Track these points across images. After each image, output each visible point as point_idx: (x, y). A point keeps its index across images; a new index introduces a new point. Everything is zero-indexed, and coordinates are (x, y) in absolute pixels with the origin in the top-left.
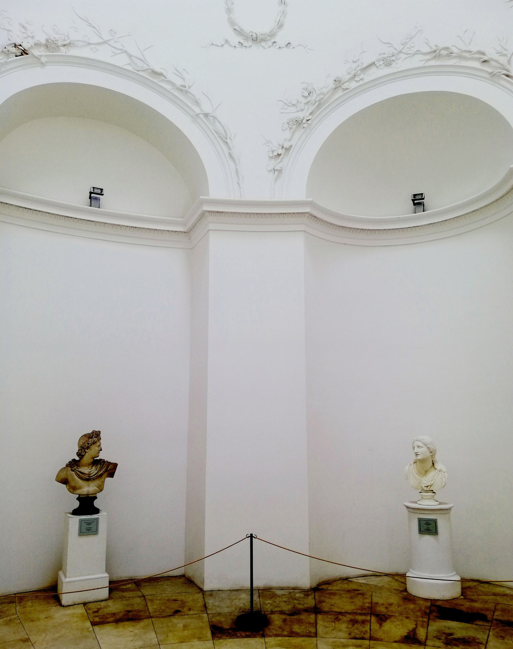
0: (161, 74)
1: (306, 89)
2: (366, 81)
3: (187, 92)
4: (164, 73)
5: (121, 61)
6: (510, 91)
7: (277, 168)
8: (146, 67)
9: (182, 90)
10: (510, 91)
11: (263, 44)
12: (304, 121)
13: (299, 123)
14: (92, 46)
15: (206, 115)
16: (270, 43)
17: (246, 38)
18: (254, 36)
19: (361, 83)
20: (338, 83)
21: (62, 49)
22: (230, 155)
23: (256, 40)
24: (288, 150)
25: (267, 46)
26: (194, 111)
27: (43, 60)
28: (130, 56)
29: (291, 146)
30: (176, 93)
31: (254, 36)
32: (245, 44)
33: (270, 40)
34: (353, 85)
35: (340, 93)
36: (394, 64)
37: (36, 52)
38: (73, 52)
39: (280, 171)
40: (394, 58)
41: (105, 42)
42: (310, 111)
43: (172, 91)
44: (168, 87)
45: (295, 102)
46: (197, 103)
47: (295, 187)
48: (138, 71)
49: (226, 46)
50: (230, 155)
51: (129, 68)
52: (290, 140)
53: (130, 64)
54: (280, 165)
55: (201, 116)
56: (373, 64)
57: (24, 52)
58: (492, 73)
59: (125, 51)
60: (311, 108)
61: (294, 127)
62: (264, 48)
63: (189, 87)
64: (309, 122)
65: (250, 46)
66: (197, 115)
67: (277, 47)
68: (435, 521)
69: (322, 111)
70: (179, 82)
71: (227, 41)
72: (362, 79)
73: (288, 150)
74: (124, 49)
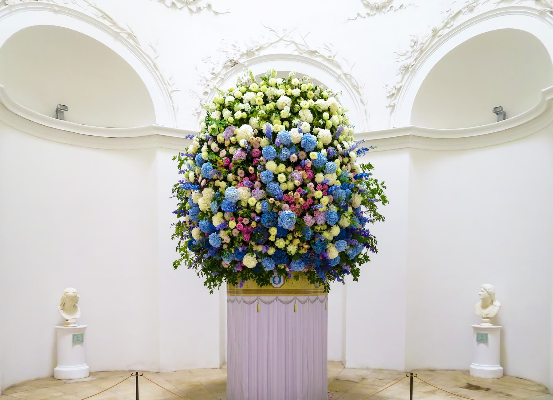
0: (316, 52)
1: (412, 41)
2: (454, 27)
3: (333, 60)
4: (318, 51)
5: (291, 50)
6: (551, 24)
7: (392, 104)
8: (307, 50)
9: (329, 60)
10: (551, 24)
11: (383, 10)
12: (410, 66)
13: (407, 68)
14: (273, 45)
15: (345, 75)
16: (388, 8)
17: (372, 9)
18: (377, 6)
19: (452, 28)
20: (435, 32)
21: (256, 53)
22: (362, 101)
23: (378, 9)
24: (399, 89)
25: (386, 11)
26: (337, 74)
27: (246, 64)
28: (296, 44)
29: (401, 87)
30: (326, 63)
31: (377, 6)
32: (372, 13)
33: (388, 6)
34: (446, 31)
35: (436, 39)
36: (475, 9)
37: (241, 61)
38: (263, 53)
39: (394, 106)
40: (475, 4)
41: (281, 39)
42: (414, 58)
43: (323, 62)
44: (319, 60)
45: (405, 52)
46: (339, 67)
47: (403, 119)
48: (302, 54)
49: (359, 18)
50: (362, 101)
51: (296, 53)
52: (401, 82)
53: (296, 50)
54: (394, 102)
55: (342, 76)
56: (460, 12)
57: (236, 63)
58: (540, 10)
59: (293, 42)
60: (416, 54)
61: (404, 72)
62: (384, 13)
63: (334, 57)
64: (413, 67)
65: (375, 14)
66: (339, 76)
67: (394, 10)
68: (486, 335)
69: (425, 54)
70: (326, 54)
71: (359, 14)
72: (452, 26)
73: (399, 89)
74: (292, 40)
